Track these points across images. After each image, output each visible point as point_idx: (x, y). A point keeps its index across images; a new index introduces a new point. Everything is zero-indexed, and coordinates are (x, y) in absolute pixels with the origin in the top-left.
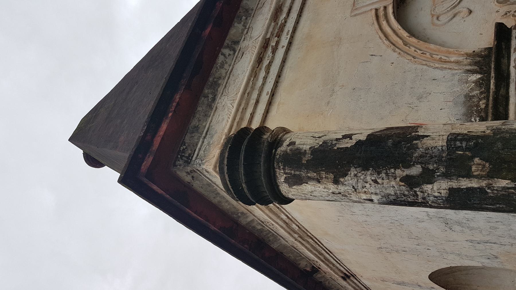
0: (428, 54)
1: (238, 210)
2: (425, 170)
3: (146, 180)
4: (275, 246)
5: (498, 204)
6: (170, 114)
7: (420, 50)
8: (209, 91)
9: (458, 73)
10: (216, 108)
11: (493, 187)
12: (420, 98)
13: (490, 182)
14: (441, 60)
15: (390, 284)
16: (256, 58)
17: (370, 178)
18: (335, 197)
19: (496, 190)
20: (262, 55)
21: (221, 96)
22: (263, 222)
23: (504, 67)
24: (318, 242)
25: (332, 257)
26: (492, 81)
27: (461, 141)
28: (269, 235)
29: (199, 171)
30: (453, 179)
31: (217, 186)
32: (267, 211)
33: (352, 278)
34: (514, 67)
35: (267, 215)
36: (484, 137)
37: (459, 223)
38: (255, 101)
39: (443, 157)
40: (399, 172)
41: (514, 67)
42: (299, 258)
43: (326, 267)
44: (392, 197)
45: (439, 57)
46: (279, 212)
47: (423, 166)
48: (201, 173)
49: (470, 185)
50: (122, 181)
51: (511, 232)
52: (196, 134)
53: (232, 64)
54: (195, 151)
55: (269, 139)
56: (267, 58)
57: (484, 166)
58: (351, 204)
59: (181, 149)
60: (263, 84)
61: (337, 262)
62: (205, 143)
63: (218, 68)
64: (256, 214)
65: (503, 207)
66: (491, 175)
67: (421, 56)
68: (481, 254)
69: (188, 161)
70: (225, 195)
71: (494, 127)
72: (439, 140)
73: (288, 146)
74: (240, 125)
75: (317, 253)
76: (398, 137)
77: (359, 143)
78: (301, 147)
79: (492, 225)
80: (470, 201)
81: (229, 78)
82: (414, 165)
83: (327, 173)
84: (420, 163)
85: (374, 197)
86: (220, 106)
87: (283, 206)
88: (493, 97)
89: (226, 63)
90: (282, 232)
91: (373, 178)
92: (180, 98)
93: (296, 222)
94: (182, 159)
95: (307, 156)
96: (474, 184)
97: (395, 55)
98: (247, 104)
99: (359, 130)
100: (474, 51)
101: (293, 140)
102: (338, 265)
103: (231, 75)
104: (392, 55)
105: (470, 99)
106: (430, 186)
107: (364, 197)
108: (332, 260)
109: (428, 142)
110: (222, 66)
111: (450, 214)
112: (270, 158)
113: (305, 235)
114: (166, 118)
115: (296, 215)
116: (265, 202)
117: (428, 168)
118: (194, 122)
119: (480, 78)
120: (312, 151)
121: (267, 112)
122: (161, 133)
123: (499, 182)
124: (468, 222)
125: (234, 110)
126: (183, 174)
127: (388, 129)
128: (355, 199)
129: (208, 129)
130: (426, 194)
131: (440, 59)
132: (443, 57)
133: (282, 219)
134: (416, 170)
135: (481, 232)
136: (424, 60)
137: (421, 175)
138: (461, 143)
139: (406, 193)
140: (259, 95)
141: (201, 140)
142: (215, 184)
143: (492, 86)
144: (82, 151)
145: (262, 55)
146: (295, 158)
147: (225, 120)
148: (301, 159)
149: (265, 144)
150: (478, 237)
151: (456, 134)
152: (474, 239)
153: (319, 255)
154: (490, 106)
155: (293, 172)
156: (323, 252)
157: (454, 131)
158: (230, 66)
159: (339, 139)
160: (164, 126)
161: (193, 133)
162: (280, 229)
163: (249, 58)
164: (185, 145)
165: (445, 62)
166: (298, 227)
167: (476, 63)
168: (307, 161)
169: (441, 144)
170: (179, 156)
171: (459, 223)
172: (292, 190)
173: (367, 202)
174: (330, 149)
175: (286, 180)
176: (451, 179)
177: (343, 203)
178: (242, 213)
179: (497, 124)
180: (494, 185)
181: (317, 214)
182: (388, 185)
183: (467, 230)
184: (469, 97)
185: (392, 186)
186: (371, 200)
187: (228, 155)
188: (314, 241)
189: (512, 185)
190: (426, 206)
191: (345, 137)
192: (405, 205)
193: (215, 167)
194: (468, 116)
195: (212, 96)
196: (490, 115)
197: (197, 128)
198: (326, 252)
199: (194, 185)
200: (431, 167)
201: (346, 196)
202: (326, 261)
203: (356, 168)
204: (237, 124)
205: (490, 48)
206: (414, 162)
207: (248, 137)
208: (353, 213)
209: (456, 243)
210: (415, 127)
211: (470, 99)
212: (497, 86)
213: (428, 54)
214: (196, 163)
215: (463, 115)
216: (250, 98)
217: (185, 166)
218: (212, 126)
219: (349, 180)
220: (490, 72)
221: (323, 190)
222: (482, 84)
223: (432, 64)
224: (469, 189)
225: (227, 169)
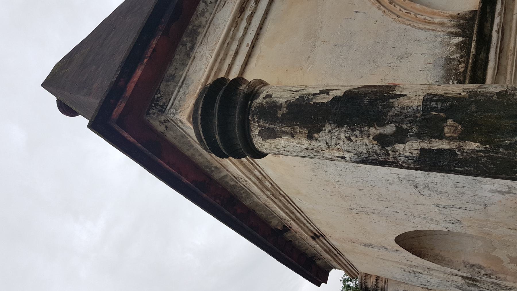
0: (413, 14)
1: (212, 164)
2: (399, 129)
3: (117, 127)
4: (247, 203)
5: (466, 166)
6: (146, 60)
7: (405, 9)
8: (188, 39)
9: (441, 35)
10: (195, 57)
11: (463, 149)
12: (400, 58)
13: (461, 144)
14: (425, 21)
15: (357, 245)
16: (238, 8)
17: (344, 135)
18: (308, 154)
19: (466, 152)
20: (244, 5)
21: (200, 45)
22: (236, 178)
23: (486, 31)
24: (290, 201)
25: (303, 216)
26: (474, 45)
27: (437, 101)
28: (242, 192)
29: (173, 120)
30: (425, 140)
31: (191, 137)
32: (240, 166)
33: (321, 238)
34: (496, 31)
35: (241, 171)
36: (460, 99)
37: (428, 187)
38: (234, 52)
39: (417, 117)
40: (372, 130)
41: (496, 31)
42: (271, 216)
43: (297, 226)
44: (364, 155)
45: (423, 17)
46: (253, 168)
47: (397, 125)
48: (175, 123)
49: (441, 147)
50: (91, 126)
51: (476, 197)
52: (172, 83)
53: (213, 13)
54: (170, 100)
55: (246, 90)
56: (249, 8)
57: (456, 128)
58: (323, 161)
59: (156, 98)
60: (244, 35)
61: (308, 221)
62: (180, 93)
63: (199, 15)
64: (229, 170)
65: (470, 170)
66: (463, 137)
67: (405, 15)
68: (446, 219)
69: (162, 110)
70: (199, 147)
71: (470, 90)
72: (415, 99)
73: (264, 98)
74: (218, 75)
75: (288, 212)
76: (375, 95)
77: (336, 99)
78: (277, 100)
79: (459, 190)
80: (440, 162)
81: (209, 27)
82: (388, 124)
83: (301, 128)
84: (394, 122)
85: (346, 155)
86: (198, 55)
87: (255, 160)
88: (473, 61)
89: (207, 11)
90: (255, 189)
91: (347, 135)
92: (157, 44)
93: (269, 179)
94: (156, 108)
95: (282, 110)
96: (445, 145)
97: (380, 13)
98: (226, 55)
99: (337, 86)
100: (459, 14)
101: (270, 93)
102: (308, 225)
103: (212, 25)
104: (377, 13)
105: (450, 61)
106: (402, 146)
107: (337, 154)
108: (303, 220)
109: (404, 102)
110: (203, 14)
111: (419, 175)
112: (246, 109)
113: (278, 193)
114: (141, 64)
115: (269, 172)
116: (238, 155)
117: (401, 128)
118: (171, 71)
119: (461, 42)
120: (288, 105)
121: (246, 64)
122: (135, 79)
123: (469, 144)
124: (437, 186)
125: (212, 60)
126: (155, 123)
127: (365, 87)
128: (328, 156)
129: (185, 78)
130: (398, 154)
131: (424, 19)
132: (427, 18)
133: (255, 175)
134: (389, 129)
135: (448, 197)
136: (408, 20)
137: (394, 134)
138: (437, 104)
139: (378, 151)
140: (239, 46)
141: (177, 89)
142: (189, 136)
143: (473, 50)
144: (55, 99)
145: (244, 5)
146: (270, 111)
147: (203, 70)
148: (276, 112)
149: (241, 95)
150: (445, 201)
151: (432, 94)
152: (441, 203)
153: (290, 214)
154: (469, 69)
155: (267, 125)
156: (295, 211)
157: (430, 92)
158: (211, 14)
159: (316, 94)
160: (139, 73)
161: (169, 81)
162: (253, 185)
163: (231, 7)
164: (159, 93)
165: (429, 23)
166: (271, 184)
167: (459, 26)
168: (282, 115)
169: (416, 104)
170: (153, 105)
171: (428, 187)
172: (265, 144)
173: (339, 159)
174: (307, 103)
175: (260, 134)
176: (423, 140)
177: (317, 161)
178: (216, 168)
179: (474, 87)
180: (464, 147)
181: (291, 171)
182: (361, 143)
183: (435, 194)
184: (448, 60)
185: (365, 144)
186: (344, 158)
187: (203, 105)
188: (286, 199)
189: (482, 148)
190: (397, 167)
191: (322, 92)
192: (376, 164)
193: (189, 117)
194: (446, 79)
195: (190, 45)
196: (468, 78)
197: (173, 76)
198: (298, 211)
199: (167, 135)
200: (405, 127)
201: (319, 152)
202: (297, 220)
203: (330, 124)
204: (214, 75)
205: (475, 12)
206: (389, 121)
207: (224, 87)
208: (326, 173)
209: (423, 207)
210: (392, 86)
211: (450, 61)
212: (477, 49)
213: (413, 14)
214: (170, 113)
215: (442, 78)
216: (229, 48)
217: (158, 115)
218: (188, 76)
219: (323, 136)
220: (473, 36)
221: (296, 145)
222: (463, 47)
223: (415, 25)
224: (439, 150)
225: (201, 119)
